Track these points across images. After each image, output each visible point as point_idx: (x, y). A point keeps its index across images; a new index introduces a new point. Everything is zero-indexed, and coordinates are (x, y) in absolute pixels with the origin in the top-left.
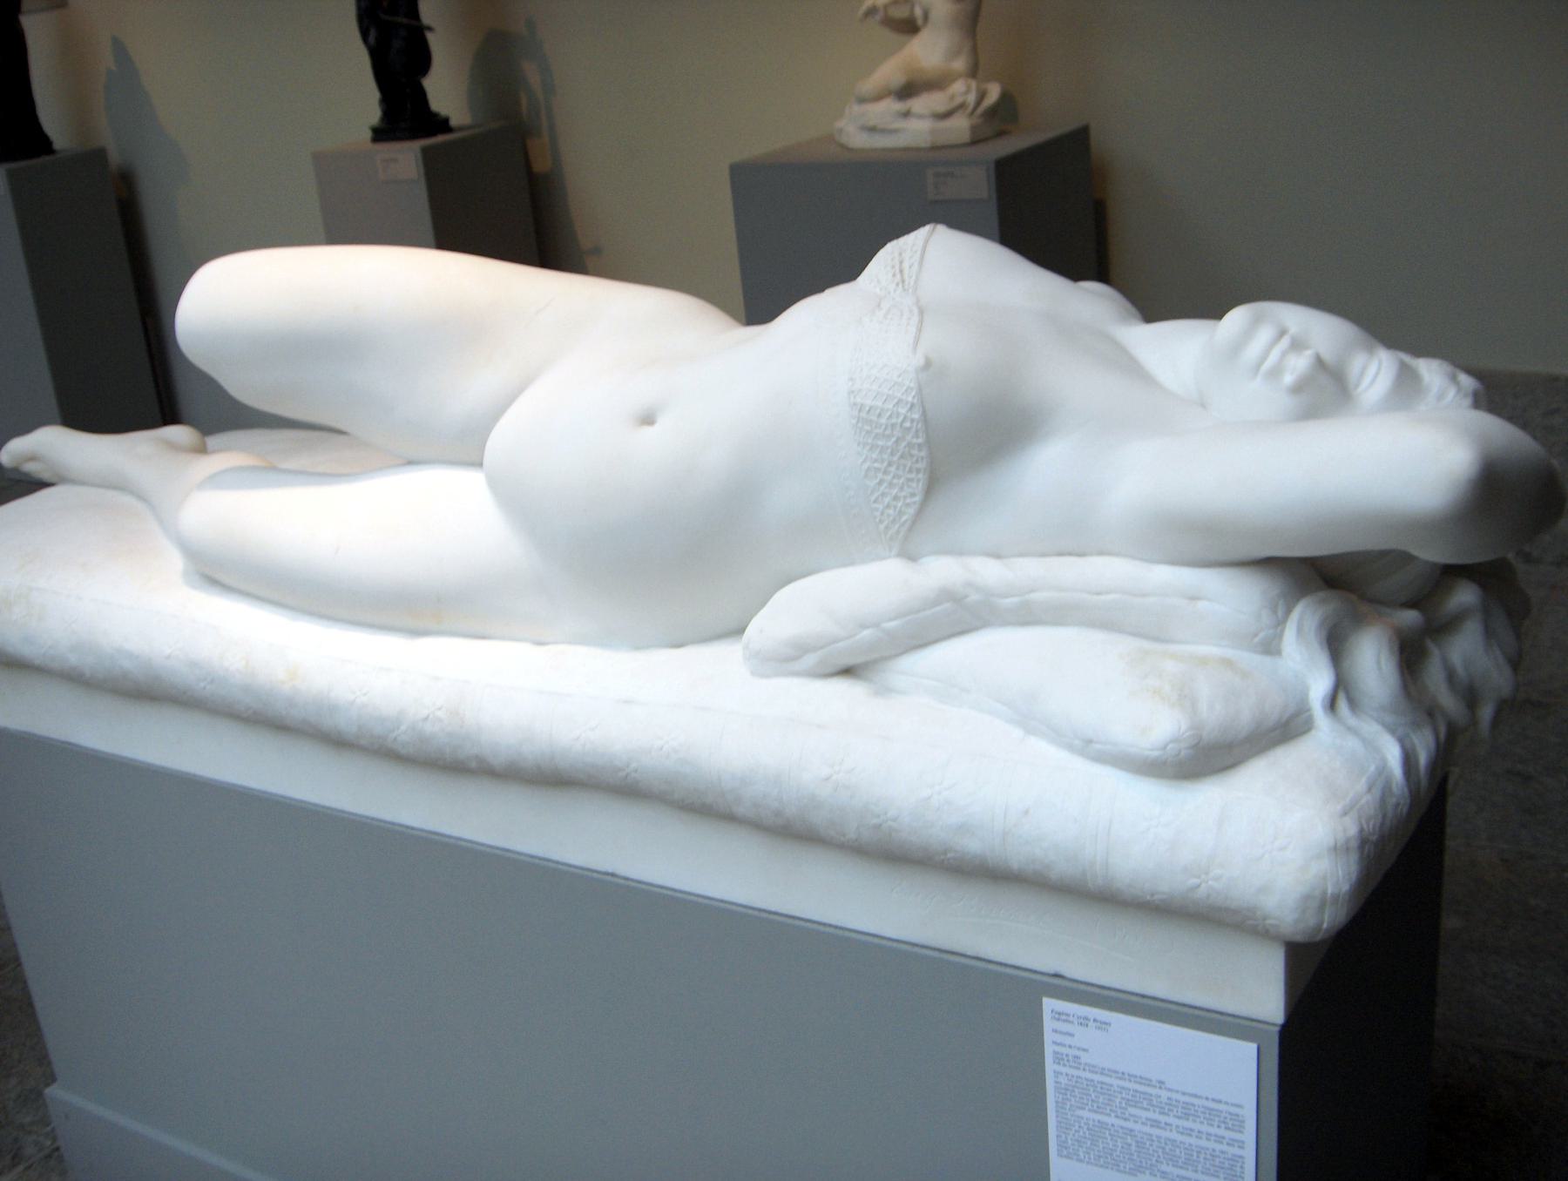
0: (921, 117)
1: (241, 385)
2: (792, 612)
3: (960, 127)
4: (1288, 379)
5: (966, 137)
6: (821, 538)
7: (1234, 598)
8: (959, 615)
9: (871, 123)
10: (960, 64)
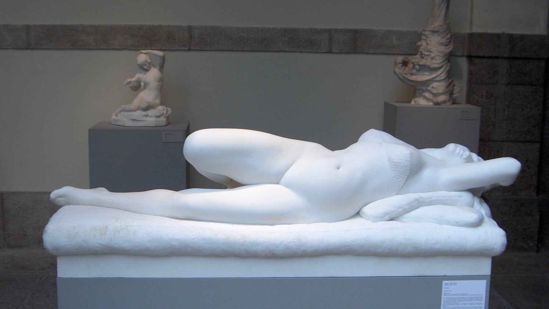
0: (151, 116)
1: (201, 168)
2: (373, 208)
3: (163, 120)
4: (464, 157)
5: (165, 124)
6: (381, 192)
7: (467, 197)
8: (417, 204)
9: (135, 118)
10: (158, 101)
